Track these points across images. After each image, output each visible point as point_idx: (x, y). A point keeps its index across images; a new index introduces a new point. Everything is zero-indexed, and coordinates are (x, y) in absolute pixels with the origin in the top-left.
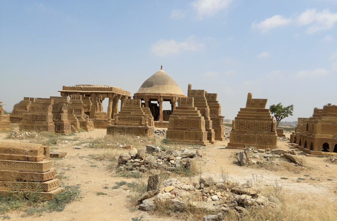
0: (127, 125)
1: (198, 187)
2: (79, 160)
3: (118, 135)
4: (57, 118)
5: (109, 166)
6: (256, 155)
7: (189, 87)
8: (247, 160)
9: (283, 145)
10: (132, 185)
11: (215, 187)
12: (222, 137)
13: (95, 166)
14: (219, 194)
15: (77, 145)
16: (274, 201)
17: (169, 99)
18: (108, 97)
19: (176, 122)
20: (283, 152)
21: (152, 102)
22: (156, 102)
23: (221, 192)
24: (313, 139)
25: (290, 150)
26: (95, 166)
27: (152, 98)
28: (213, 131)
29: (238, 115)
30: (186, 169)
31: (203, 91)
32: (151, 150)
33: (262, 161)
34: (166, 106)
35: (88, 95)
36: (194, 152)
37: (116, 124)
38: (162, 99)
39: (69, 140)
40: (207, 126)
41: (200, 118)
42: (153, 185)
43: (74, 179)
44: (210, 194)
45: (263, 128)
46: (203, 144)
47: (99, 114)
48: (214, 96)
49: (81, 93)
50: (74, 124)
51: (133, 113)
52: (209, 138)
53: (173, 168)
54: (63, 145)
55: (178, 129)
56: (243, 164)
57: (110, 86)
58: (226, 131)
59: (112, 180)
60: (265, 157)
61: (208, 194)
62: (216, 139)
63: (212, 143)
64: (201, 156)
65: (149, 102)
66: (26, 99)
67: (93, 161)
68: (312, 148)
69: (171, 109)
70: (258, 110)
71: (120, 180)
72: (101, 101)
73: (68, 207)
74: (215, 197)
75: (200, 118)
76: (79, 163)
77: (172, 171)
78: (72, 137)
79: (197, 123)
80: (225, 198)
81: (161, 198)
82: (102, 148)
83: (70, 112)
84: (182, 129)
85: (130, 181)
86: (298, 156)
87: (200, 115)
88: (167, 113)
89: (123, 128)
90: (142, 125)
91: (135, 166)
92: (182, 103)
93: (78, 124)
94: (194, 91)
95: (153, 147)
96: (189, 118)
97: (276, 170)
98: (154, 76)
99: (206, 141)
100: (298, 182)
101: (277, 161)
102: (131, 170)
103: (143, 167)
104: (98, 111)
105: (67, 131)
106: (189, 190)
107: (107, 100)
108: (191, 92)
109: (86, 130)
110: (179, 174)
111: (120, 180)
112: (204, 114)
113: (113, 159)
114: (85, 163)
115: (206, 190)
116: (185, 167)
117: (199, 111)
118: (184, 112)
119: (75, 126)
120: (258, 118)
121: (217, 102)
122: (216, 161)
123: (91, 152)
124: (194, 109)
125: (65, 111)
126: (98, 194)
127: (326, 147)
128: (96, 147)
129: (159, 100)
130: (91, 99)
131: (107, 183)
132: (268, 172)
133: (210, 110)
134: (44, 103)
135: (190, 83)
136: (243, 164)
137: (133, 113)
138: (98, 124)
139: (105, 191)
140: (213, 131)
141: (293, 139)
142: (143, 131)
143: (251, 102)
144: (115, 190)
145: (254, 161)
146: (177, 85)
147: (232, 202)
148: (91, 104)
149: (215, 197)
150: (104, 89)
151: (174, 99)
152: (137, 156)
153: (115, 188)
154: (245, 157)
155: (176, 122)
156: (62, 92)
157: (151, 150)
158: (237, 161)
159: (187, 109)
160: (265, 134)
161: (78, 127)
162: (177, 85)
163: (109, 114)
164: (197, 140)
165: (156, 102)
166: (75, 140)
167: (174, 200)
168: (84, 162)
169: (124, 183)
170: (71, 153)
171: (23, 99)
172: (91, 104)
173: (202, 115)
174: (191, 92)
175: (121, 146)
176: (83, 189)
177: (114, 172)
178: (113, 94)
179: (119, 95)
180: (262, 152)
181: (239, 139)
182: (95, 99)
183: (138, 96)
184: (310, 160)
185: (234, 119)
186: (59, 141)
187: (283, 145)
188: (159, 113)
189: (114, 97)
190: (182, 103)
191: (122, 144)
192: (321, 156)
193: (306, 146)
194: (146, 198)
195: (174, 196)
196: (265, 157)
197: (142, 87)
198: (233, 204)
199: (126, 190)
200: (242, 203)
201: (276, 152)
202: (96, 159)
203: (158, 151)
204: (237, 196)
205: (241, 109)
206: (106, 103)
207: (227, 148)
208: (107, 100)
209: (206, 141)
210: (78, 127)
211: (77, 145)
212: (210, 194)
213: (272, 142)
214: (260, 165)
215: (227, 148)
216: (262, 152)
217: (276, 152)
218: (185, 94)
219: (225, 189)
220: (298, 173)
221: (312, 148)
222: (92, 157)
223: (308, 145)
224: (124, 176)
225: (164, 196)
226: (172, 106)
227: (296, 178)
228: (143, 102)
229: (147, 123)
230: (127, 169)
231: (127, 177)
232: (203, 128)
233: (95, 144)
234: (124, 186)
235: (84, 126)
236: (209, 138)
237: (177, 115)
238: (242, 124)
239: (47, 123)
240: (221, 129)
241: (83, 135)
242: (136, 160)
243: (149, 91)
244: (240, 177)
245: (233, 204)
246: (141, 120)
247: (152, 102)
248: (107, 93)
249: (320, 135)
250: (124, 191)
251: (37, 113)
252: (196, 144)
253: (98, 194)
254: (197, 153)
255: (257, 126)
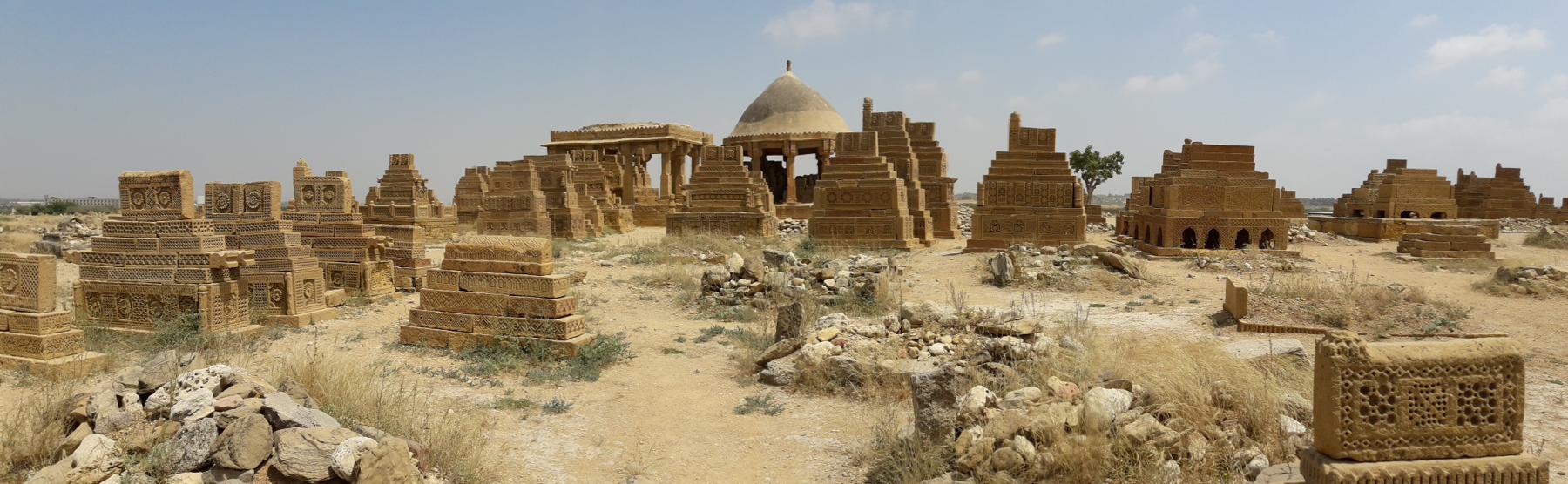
0: (711, 209)
1: (897, 328)
2: (613, 287)
3: (691, 234)
4: (554, 204)
5: (680, 298)
6: (1035, 260)
7: (867, 105)
8: (1017, 271)
9: (1098, 238)
10: (739, 335)
11: (936, 326)
12: (954, 228)
13: (650, 299)
14: (947, 339)
15: (605, 258)
16: (1072, 348)
17: (812, 146)
18: (658, 152)
19: (832, 197)
20: (1097, 250)
21: (770, 158)
22: (779, 158)
23: (953, 334)
24: (1163, 220)
25: (1112, 246)
26: (650, 299)
27: (769, 146)
28: (927, 216)
29: (991, 170)
30: (865, 296)
31: (900, 115)
32: (776, 260)
33: (1049, 273)
34: (805, 165)
35: (611, 150)
36: (883, 261)
37: (685, 209)
38: (793, 148)
39: (585, 250)
40: (913, 202)
41: (894, 182)
42: (790, 327)
43: (610, 323)
44: (926, 341)
45: (1053, 199)
46: (903, 247)
47: (643, 192)
48: (929, 128)
49: (596, 146)
50: (591, 216)
51: (723, 180)
52: (919, 232)
53: (833, 297)
54: (576, 260)
55: (837, 213)
56: (1008, 282)
57: (663, 124)
58: (962, 216)
59: (693, 328)
60: (1056, 264)
61: (921, 342)
62: (936, 235)
63: (927, 244)
64: (900, 272)
65: (763, 158)
66: (469, 172)
67: (642, 289)
68: (1160, 244)
69: (815, 172)
70: (1041, 156)
71: (709, 324)
72: (644, 163)
73: (608, 374)
74: (937, 347)
75: (894, 182)
76: (614, 294)
77: (831, 303)
78: (591, 245)
79: (888, 194)
80: (963, 347)
81: (811, 354)
82: (659, 262)
83: (580, 189)
84: (850, 213)
85: (731, 326)
86: (1130, 258)
87: (893, 175)
88: (807, 182)
89: (702, 217)
90: (747, 209)
91: (740, 295)
92: (848, 147)
93: (600, 216)
94: (879, 115)
95: (780, 253)
96: (867, 183)
97: (1081, 290)
98: (771, 90)
99: (911, 241)
100: (1127, 309)
101: (1083, 270)
102: (733, 304)
103: (759, 297)
104: (640, 186)
105: (579, 233)
106: (875, 335)
107: (657, 159)
108: (872, 120)
109: (617, 229)
110: (849, 309)
111: (709, 324)
112: (903, 171)
113: (686, 285)
114: (629, 292)
115: (916, 333)
116: (863, 293)
117: (890, 166)
118: (850, 169)
119: (595, 221)
120: (1039, 175)
121: (935, 143)
122: (938, 276)
123: (637, 270)
124: (879, 160)
125: (570, 186)
126: (667, 351)
127: (1189, 239)
128: (647, 262)
129: (786, 152)
130: (620, 160)
131: (681, 330)
132: (1064, 294)
133: (920, 165)
134: (515, 172)
135: (869, 97)
136: (1008, 282)
137: (723, 180)
138: (644, 217)
139: (678, 346)
140: (927, 216)
141: (1123, 227)
142: (753, 224)
143: (1019, 134)
144: (702, 345)
145: (1032, 274)
146: (832, 109)
147: (978, 354)
148: (622, 172)
149: (937, 347)
150: (649, 132)
151: (826, 145)
152: (744, 273)
153: (702, 340)
154: (1010, 265)
155: (832, 197)
156: (549, 147)
157: (776, 260)
158: (991, 276)
159: (861, 161)
160: (1058, 213)
161: (601, 223)
162: (832, 109)
163: (664, 190)
164: (890, 238)
165: (779, 158)
166: (597, 250)
167: (838, 358)
168: (623, 290)
169: (719, 331)
170: (594, 273)
171: (386, 165)
172: (622, 172)
173: (900, 176)
174: (872, 120)
175: (703, 256)
176: (634, 341)
177: (694, 309)
178: (671, 141)
179: (685, 144)
180: (1051, 253)
181: (996, 227)
182: (629, 159)
183: (730, 142)
184: (1156, 268)
185: (981, 181)
186: (565, 249)
187: (1098, 238)
188: (786, 184)
189: (673, 149)
190: (848, 147)
191: (705, 252)
192: (1177, 258)
193: (1147, 240)
194: (776, 355)
195: (839, 348)
196: (1056, 264)
197: (742, 120)
198: (981, 359)
199: (725, 344)
200: (997, 354)
201: (1082, 252)
202: (651, 285)
203: (792, 263)
204: (989, 341)
205: (999, 154)
206: (655, 167)
207: (965, 251)
208: (657, 159)
209: (911, 241)
210: (601, 223)
211: (605, 258)
212: (926, 341)
213: (1075, 232)
214: (1045, 282)
215: (965, 251)
216: (1051, 253)
217: (1082, 252)
218: (857, 127)
219: (963, 327)
220: (1129, 293)
221: (1160, 244)
222: (641, 280)
223: (1153, 236)
224: (717, 317)
225: (817, 346)
226: (820, 165)
227: (1123, 304)
228: (748, 159)
229: (760, 203)
230: (723, 303)
231: (725, 319)
232: (903, 208)
233: (642, 256)
234: (718, 338)
235: (612, 220)
236: (919, 232)
237: (835, 176)
238: (1002, 191)
239: (534, 215)
240: (948, 211)
241: (613, 239)
242: (742, 281)
243: (760, 130)
244: (993, 303)
245: (981, 359)
246: (744, 197)
247: (770, 158)
248: (656, 142)
249: (1179, 211)
250: (722, 347)
251: (512, 194)
252: (887, 246)
253: (667, 351)
254: (890, 262)
255: (1036, 192)
